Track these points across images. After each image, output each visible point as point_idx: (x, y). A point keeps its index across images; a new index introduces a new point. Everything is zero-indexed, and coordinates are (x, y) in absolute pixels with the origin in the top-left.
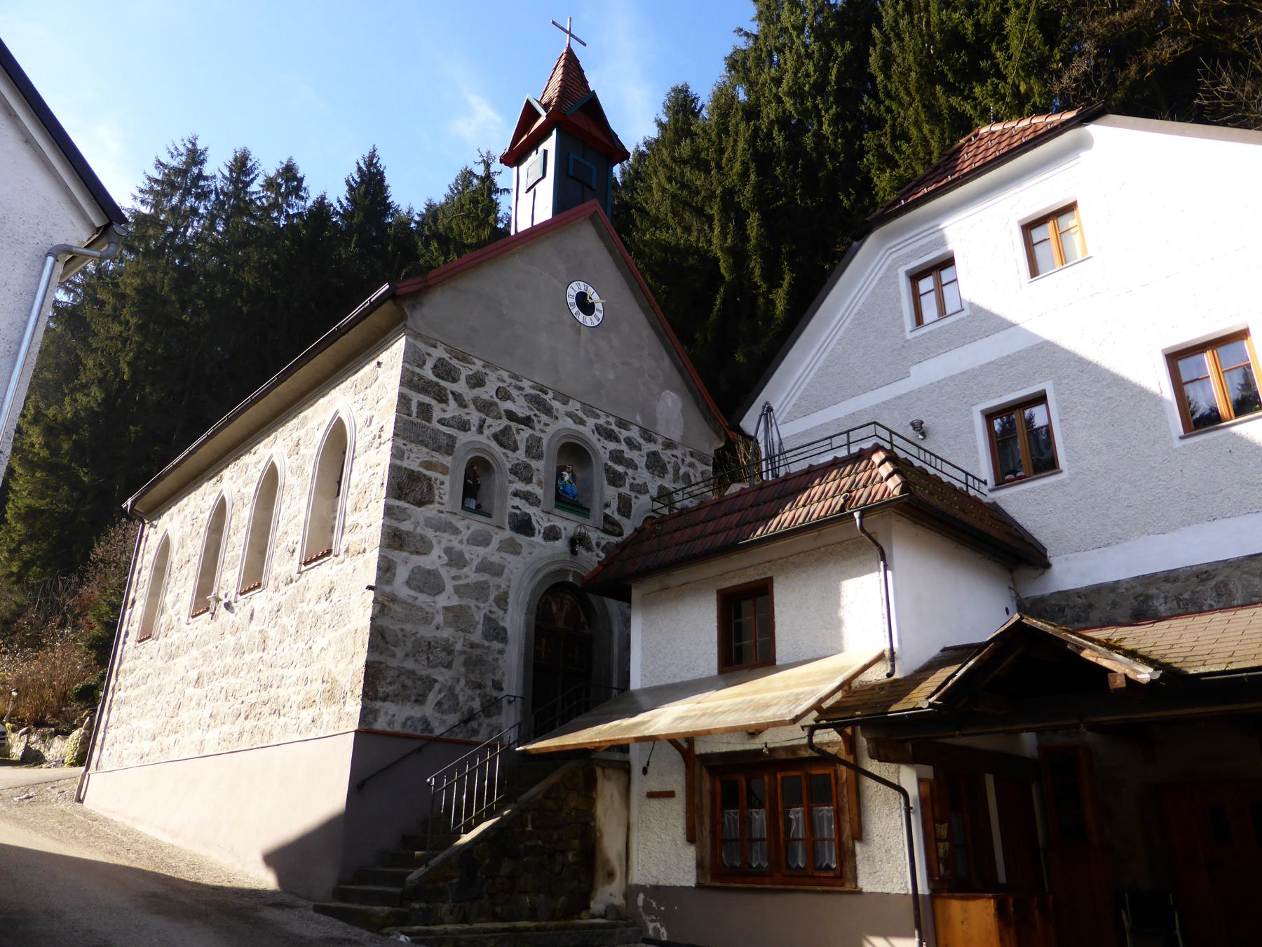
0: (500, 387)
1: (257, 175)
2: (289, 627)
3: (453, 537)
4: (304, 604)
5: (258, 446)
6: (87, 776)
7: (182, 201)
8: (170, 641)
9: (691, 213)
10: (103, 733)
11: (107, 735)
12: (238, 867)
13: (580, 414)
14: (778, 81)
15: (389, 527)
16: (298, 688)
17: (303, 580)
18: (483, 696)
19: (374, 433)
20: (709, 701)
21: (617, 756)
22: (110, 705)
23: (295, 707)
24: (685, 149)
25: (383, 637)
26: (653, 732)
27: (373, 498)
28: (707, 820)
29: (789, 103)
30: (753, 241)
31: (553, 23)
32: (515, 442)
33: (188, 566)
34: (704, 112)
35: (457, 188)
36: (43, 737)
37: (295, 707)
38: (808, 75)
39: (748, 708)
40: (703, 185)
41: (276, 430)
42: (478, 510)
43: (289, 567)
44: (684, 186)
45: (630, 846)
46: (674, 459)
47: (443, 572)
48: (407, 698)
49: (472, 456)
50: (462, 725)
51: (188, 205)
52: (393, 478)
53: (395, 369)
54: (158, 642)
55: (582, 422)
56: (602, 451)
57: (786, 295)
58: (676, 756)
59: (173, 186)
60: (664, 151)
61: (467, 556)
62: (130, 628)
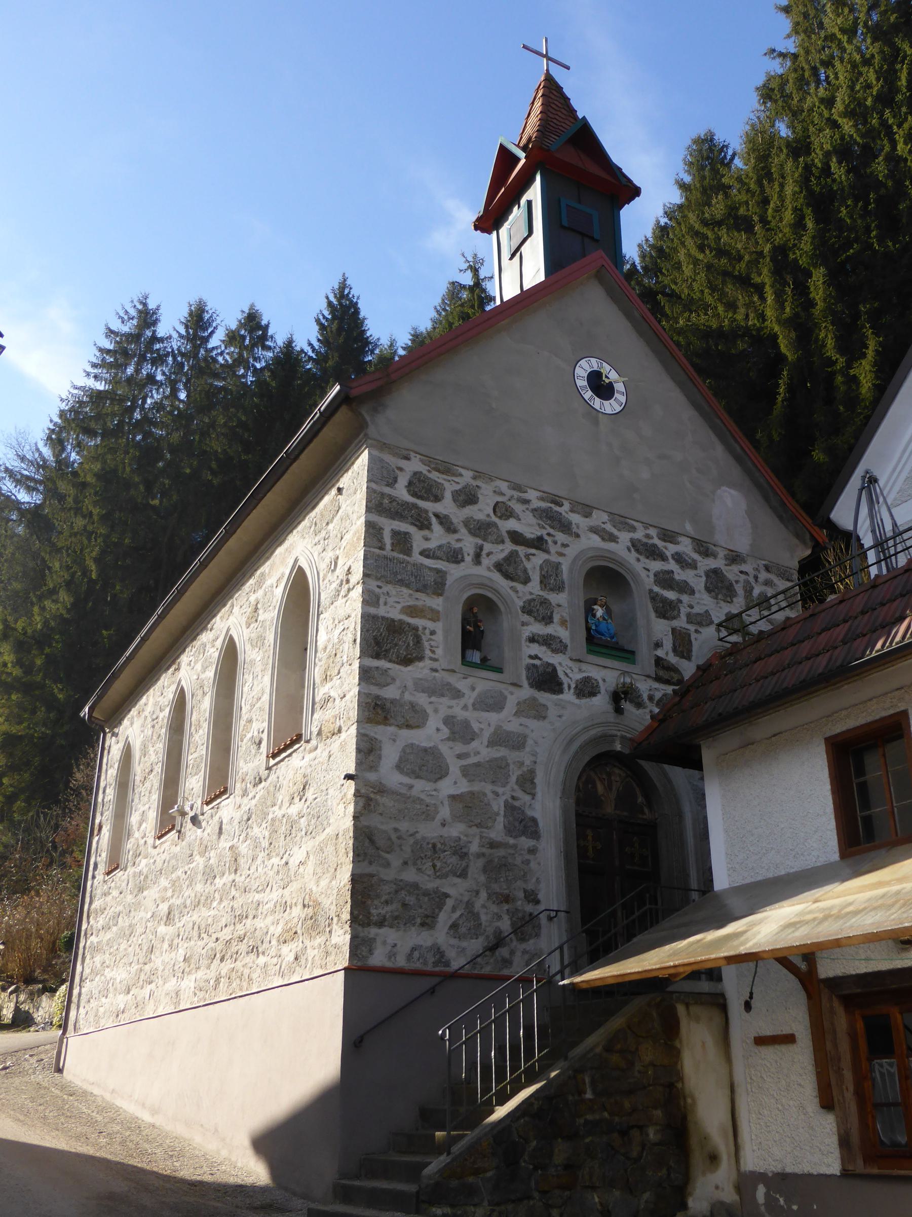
0: (497, 503)
1: (216, 328)
2: (261, 839)
3: (453, 702)
4: (276, 808)
5: (214, 620)
6: (65, 1040)
7: (138, 371)
8: (137, 870)
9: (734, 284)
10: (78, 988)
11: (83, 990)
12: (224, 1153)
13: (609, 527)
14: (829, 102)
15: (368, 695)
16: (277, 916)
17: (273, 777)
18: (512, 913)
19: (341, 577)
20: (833, 898)
21: (705, 986)
22: (84, 954)
23: (274, 942)
24: (718, 207)
25: (372, 841)
26: (751, 947)
27: (345, 661)
28: (848, 1075)
29: (847, 126)
30: (820, 305)
31: (525, 47)
32: (525, 571)
33: (151, 776)
34: (738, 163)
35: (444, 310)
36: (31, 996)
37: (274, 942)
38: (869, 86)
39: (896, 902)
40: (746, 248)
41: (231, 597)
42: (485, 664)
43: (256, 763)
44: (721, 252)
45: (737, 1115)
46: (743, 577)
47: (444, 749)
48: (410, 921)
49: (469, 593)
50: (487, 953)
51: (145, 373)
52: (368, 631)
53: (359, 491)
54: (126, 873)
55: (613, 538)
56: (643, 574)
57: (873, 367)
58: (791, 982)
59: (125, 353)
60: (690, 215)
61: (475, 726)
62: (99, 859)
